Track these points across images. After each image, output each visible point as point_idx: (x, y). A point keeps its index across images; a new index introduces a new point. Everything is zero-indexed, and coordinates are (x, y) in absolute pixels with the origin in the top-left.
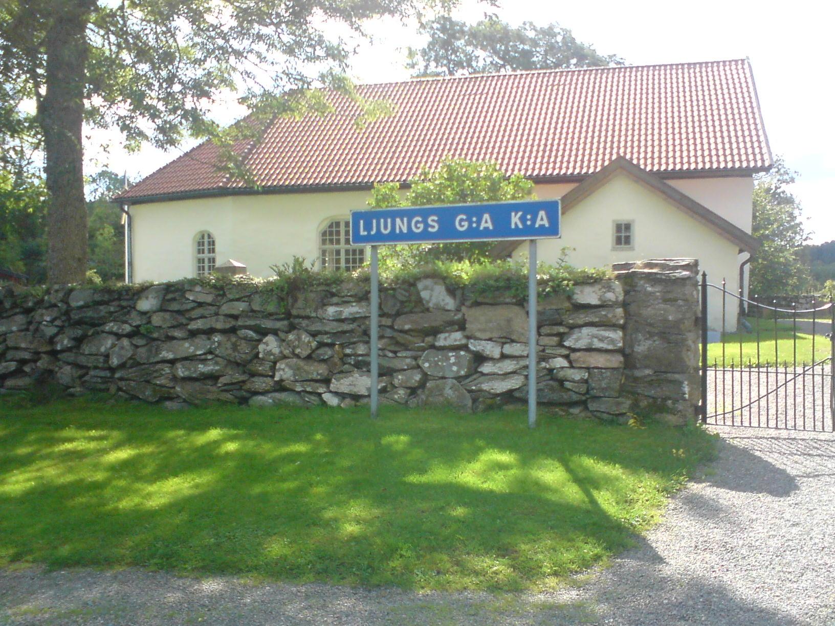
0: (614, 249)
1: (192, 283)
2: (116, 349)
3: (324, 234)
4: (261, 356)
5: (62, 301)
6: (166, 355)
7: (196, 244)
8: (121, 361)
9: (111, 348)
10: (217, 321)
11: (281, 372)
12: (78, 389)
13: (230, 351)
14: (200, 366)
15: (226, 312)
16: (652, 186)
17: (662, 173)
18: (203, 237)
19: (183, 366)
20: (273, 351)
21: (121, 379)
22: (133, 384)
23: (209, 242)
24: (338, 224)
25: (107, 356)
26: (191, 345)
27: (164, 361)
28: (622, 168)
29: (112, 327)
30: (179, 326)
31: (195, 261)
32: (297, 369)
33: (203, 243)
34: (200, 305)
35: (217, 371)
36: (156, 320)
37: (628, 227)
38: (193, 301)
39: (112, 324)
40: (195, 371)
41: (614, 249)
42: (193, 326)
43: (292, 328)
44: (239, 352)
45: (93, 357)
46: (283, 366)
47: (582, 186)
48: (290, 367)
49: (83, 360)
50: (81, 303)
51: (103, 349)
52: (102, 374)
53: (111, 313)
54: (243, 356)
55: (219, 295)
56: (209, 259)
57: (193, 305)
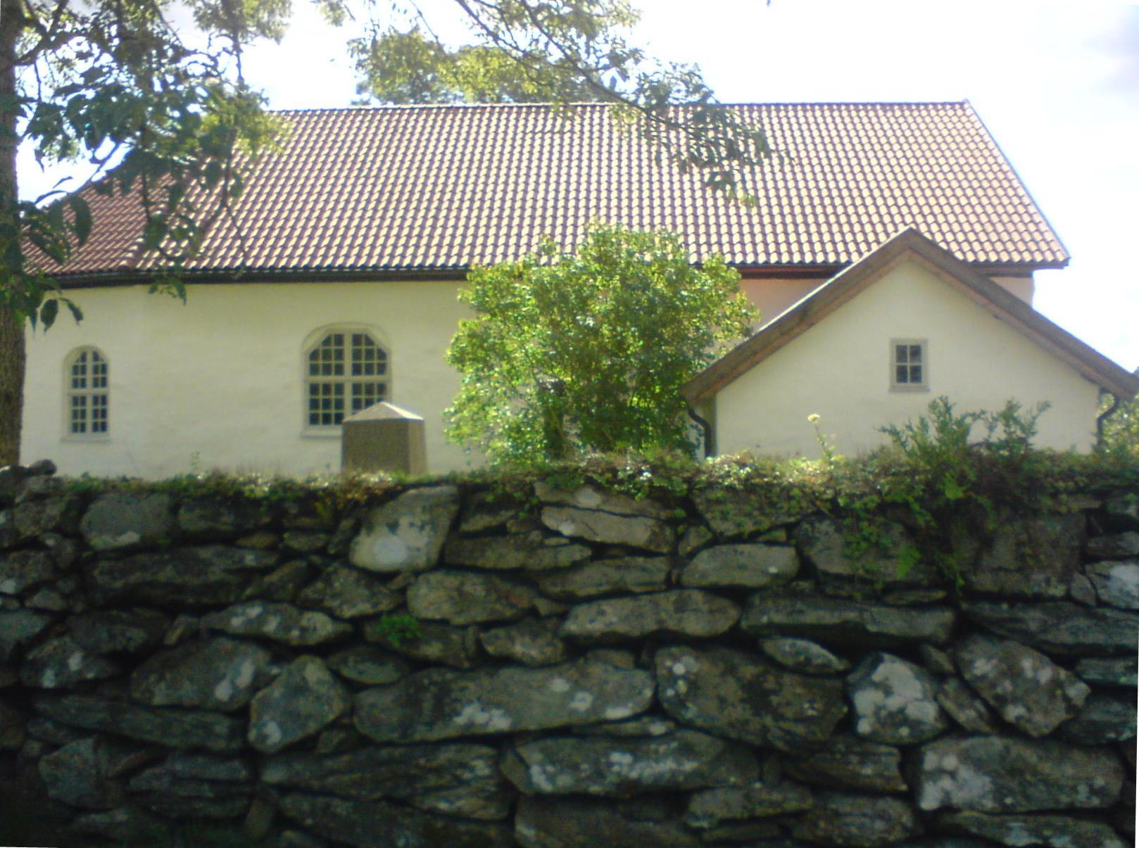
0: (893, 389)
2: (276, 692)
3: (314, 355)
4: (864, 727)
5: (57, 530)
6: (481, 718)
8: (298, 735)
9: (255, 687)
10: (681, 607)
11: (946, 783)
12: (121, 816)
13: (739, 712)
14: (616, 757)
15: (713, 579)
17: (773, 266)
18: (83, 358)
19: (550, 758)
20: (913, 711)
21: (284, 789)
22: (341, 808)
23: (96, 370)
24: (339, 339)
25: (240, 714)
26: (577, 686)
27: (472, 738)
28: (914, 250)
29: (261, 619)
30: (528, 619)
32: (1007, 773)
33: (84, 370)
34: (601, 551)
35: (689, 776)
36: (430, 599)
37: (916, 351)
38: (574, 540)
39: (255, 611)
40: (599, 775)
41: (893, 389)
42: (584, 622)
43: (966, 629)
44: (779, 717)
45: (190, 718)
46: (950, 762)
47: (818, 289)
48: (979, 765)
49: (141, 724)
50: (131, 537)
51: (222, 692)
52: (221, 771)
53: (248, 575)
54: (800, 729)
55: (673, 522)
57: (578, 553)
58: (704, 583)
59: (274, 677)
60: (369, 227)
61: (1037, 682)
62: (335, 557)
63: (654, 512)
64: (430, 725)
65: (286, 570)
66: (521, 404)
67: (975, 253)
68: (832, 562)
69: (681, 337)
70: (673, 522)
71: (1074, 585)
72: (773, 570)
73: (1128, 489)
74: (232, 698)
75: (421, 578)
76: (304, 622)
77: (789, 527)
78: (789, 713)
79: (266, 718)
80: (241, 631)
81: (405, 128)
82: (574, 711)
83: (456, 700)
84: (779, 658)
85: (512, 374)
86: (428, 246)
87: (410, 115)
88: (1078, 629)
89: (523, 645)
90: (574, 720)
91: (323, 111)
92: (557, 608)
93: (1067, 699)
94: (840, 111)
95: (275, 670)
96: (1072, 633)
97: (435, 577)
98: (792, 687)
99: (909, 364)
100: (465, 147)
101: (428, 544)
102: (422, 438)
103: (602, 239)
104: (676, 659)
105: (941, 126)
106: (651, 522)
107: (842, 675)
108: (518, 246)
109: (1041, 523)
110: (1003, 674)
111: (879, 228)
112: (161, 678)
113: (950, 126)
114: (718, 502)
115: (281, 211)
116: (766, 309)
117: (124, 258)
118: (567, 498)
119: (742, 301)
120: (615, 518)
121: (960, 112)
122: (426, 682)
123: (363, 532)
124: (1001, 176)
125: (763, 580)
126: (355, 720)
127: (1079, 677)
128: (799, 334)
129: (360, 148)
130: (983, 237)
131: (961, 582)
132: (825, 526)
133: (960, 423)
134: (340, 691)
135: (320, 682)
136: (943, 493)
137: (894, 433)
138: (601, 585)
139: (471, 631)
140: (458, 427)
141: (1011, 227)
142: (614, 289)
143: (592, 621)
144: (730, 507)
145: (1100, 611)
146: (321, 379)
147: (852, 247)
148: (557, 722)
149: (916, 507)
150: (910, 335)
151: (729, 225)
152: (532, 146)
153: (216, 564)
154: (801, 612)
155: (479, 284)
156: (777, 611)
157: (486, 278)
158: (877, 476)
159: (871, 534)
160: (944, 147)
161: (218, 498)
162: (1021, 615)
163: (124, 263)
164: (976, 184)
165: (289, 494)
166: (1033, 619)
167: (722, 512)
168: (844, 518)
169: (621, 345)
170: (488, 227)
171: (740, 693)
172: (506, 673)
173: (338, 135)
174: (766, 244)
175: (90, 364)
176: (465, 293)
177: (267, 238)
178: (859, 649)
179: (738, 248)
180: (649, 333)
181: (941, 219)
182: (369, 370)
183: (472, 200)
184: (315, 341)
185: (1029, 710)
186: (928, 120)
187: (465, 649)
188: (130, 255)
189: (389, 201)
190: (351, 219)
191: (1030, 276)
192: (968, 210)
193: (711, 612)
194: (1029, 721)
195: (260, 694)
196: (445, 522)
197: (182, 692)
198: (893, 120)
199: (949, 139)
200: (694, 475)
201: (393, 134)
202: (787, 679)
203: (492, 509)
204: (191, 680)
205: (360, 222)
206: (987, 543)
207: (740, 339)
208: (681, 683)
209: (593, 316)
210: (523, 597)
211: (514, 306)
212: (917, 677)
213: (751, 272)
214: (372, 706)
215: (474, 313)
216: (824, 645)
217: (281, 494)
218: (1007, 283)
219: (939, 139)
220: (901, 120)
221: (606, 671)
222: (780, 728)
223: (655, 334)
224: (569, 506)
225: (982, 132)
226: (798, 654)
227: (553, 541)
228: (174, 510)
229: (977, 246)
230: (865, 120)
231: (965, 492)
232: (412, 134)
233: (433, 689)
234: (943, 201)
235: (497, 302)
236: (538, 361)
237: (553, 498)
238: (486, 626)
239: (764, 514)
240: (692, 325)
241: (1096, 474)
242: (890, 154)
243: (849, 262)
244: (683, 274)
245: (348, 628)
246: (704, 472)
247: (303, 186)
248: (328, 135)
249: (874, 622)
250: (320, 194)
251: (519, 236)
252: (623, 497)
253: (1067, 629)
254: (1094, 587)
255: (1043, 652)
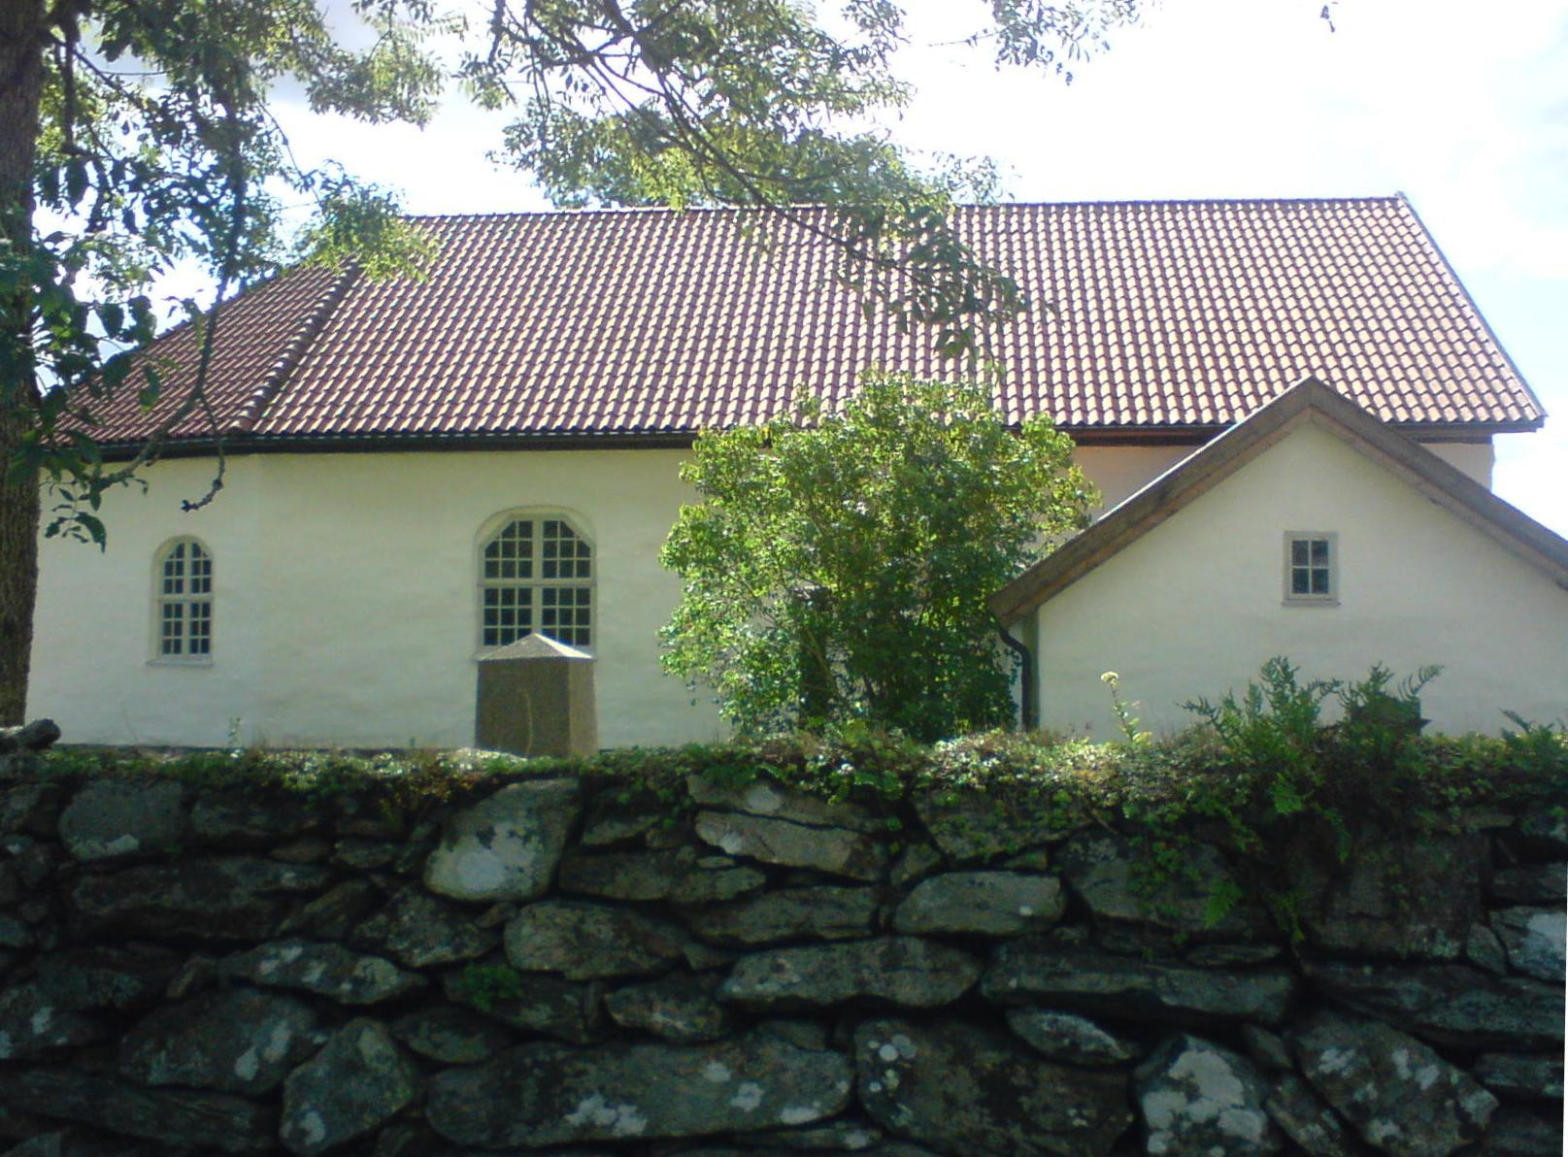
0: (1288, 602)
1: (727, 771)
2: (320, 1069)
3: (492, 550)
5: (24, 831)
6: (604, 1116)
7: (161, 570)
9: (291, 1061)
10: (892, 962)
13: (972, 1119)
15: (939, 922)
16: (1389, 453)
18: (180, 552)
20: (1229, 1123)
23: (196, 569)
24: (526, 528)
25: (269, 1099)
26: (741, 1074)
28: (1316, 407)
29: (300, 965)
30: (672, 978)
31: (158, 610)
33: (180, 566)
34: (779, 878)
36: (536, 942)
37: (1321, 549)
38: (742, 861)
39: (292, 953)
41: (1288, 602)
42: (753, 982)
43: (1309, 1004)
44: (1031, 1127)
45: (198, 1104)
47: (1185, 461)
50: (126, 843)
51: (246, 1067)
53: (286, 900)
55: (884, 837)
56: (195, 608)
57: (746, 880)
58: (926, 927)
59: (320, 1047)
60: (570, 376)
61: (1417, 1086)
62: (406, 878)
63: (857, 821)
64: (533, 1124)
65: (335, 896)
66: (765, 621)
67: (1409, 410)
68: (1113, 903)
69: (989, 532)
70: (884, 837)
71: (1472, 941)
72: (1026, 911)
73: (1551, 800)
74: (259, 1074)
75: (525, 911)
76: (358, 972)
77: (1052, 849)
78: (1046, 1121)
79: (305, 1106)
80: (273, 980)
81: (624, 239)
82: (735, 1112)
83: (568, 1090)
84: (1033, 1041)
85: (752, 581)
86: (649, 402)
87: (631, 222)
88: (1478, 1007)
89: (664, 1013)
90: (738, 1124)
91: (513, 216)
92: (718, 960)
93: (1462, 1115)
94: (1223, 213)
95: (319, 1039)
96: (1469, 1014)
97: (549, 908)
98: (1051, 1085)
99: (1310, 567)
100: (704, 265)
101: (534, 863)
102: (589, 685)
103: (881, 394)
104: (885, 1040)
105: (1364, 232)
106: (851, 836)
107: (1127, 1066)
108: (771, 400)
109: (1420, 848)
110: (1364, 1074)
111: (1274, 375)
112: (161, 1045)
113: (1377, 231)
114: (948, 808)
115: (452, 353)
116: (1108, 487)
117: (236, 418)
118: (737, 803)
119: (1077, 480)
120: (801, 829)
121: (1391, 213)
122: (528, 1061)
123: (443, 845)
124: (1447, 301)
125: (1012, 926)
126: (429, 1114)
127: (1480, 1081)
128: (1154, 526)
129: (561, 267)
130: (1420, 387)
131: (1299, 936)
132: (1104, 847)
133: (1305, 696)
134: (408, 1071)
135: (378, 1057)
136: (1272, 804)
137: (1204, 709)
138: (777, 927)
139: (592, 989)
140: (679, 653)
141: (1460, 373)
142: (895, 464)
143: (762, 981)
144: (964, 816)
145: (1514, 982)
146: (500, 582)
147: (1235, 401)
148: (711, 1126)
149: (1236, 822)
150: (1312, 524)
151: (1064, 372)
152: (796, 263)
153: (242, 883)
154: (1066, 974)
155: (708, 455)
156: (1031, 973)
157: (719, 448)
158: (1183, 772)
159: (1170, 861)
160: (1367, 260)
161: (247, 790)
162: (1391, 984)
163: (236, 423)
164: (1411, 313)
165: (345, 787)
166: (1410, 992)
167: (954, 825)
168: (1131, 836)
169: (906, 540)
170: (731, 375)
171: (976, 1091)
172: (642, 1052)
173: (532, 249)
174: (1115, 398)
175: (188, 560)
176: (690, 468)
177: (431, 390)
178: (1152, 1030)
179: (1075, 403)
180: (945, 523)
181: (1361, 361)
182: (566, 572)
183: (711, 339)
184: (492, 531)
185: (1404, 1128)
186: (1346, 223)
187: (585, 1018)
188: (245, 413)
189: (598, 340)
190: (546, 364)
191: (1489, 441)
192: (1400, 349)
193: (935, 970)
194: (1405, 1144)
195: (298, 1071)
196: (559, 832)
197: (191, 1066)
198: (1296, 224)
199: (1375, 250)
200: (916, 769)
201: (607, 248)
202: (1045, 1072)
203: (626, 813)
204: (203, 1050)
205: (558, 370)
206: (1340, 877)
207: (1073, 532)
208: (890, 1073)
209: (867, 501)
210: (667, 940)
211: (756, 486)
212: (1237, 1072)
213: (1086, 436)
214: (453, 1094)
215: (701, 495)
216: (1101, 1023)
217: (335, 786)
218: (1450, 454)
219: (1361, 251)
220: (1308, 224)
221: (785, 1052)
222: (1033, 1144)
223: (954, 524)
224: (736, 811)
225: (1422, 239)
226: (1061, 1035)
227: (711, 862)
228: (187, 804)
229: (1411, 401)
230: (1258, 224)
231: (1306, 802)
232: (633, 248)
233: (536, 1071)
234: (1364, 337)
235: (731, 482)
236: (790, 561)
237: (715, 800)
238: (614, 983)
239: (1012, 828)
240: (1004, 513)
241: (1507, 776)
242: (1291, 272)
243: (1230, 422)
244: (994, 439)
245: (421, 981)
246: (931, 764)
247: (483, 319)
248: (519, 250)
249: (1174, 992)
250: (505, 330)
251: (774, 387)
252: (812, 800)
253: (1461, 1009)
254: (1502, 944)
255: (1426, 1041)
